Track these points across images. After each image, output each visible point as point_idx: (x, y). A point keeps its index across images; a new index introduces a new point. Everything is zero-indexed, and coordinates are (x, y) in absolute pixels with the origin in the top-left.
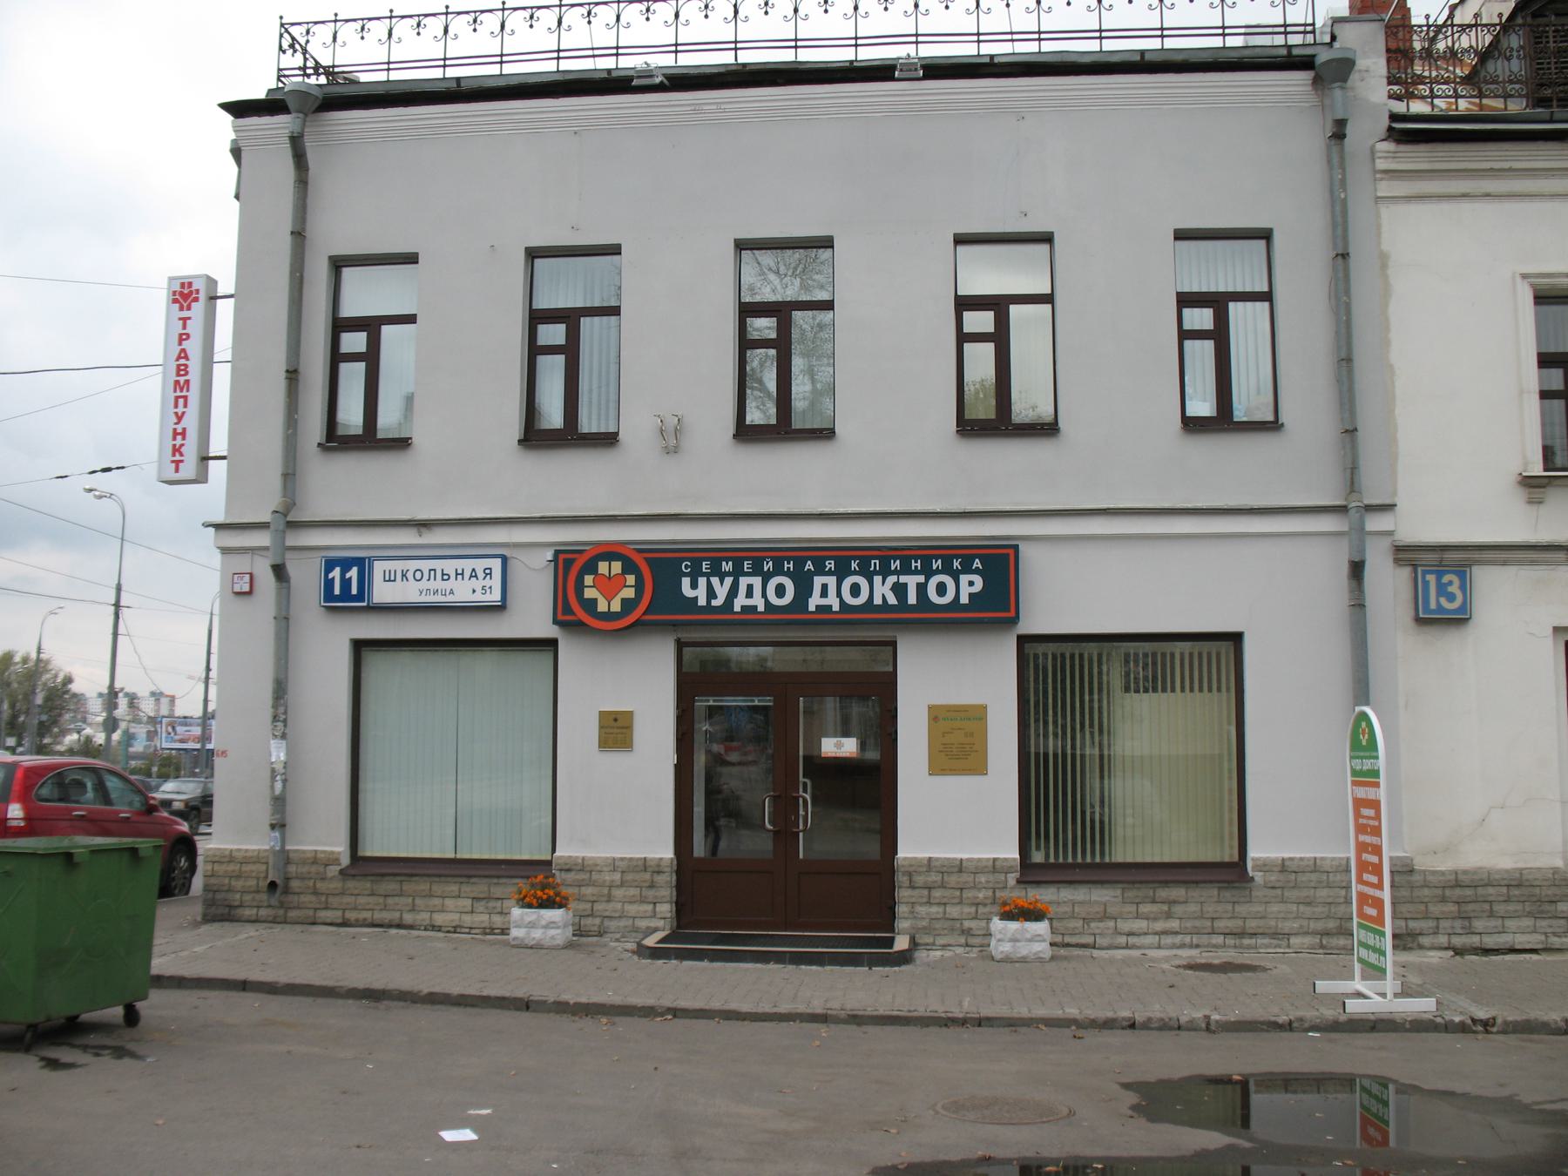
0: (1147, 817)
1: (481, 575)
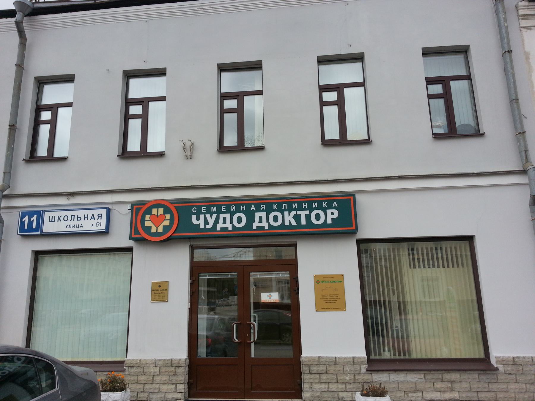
0: (431, 333)
1: (96, 217)
